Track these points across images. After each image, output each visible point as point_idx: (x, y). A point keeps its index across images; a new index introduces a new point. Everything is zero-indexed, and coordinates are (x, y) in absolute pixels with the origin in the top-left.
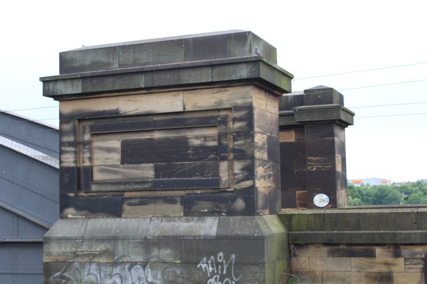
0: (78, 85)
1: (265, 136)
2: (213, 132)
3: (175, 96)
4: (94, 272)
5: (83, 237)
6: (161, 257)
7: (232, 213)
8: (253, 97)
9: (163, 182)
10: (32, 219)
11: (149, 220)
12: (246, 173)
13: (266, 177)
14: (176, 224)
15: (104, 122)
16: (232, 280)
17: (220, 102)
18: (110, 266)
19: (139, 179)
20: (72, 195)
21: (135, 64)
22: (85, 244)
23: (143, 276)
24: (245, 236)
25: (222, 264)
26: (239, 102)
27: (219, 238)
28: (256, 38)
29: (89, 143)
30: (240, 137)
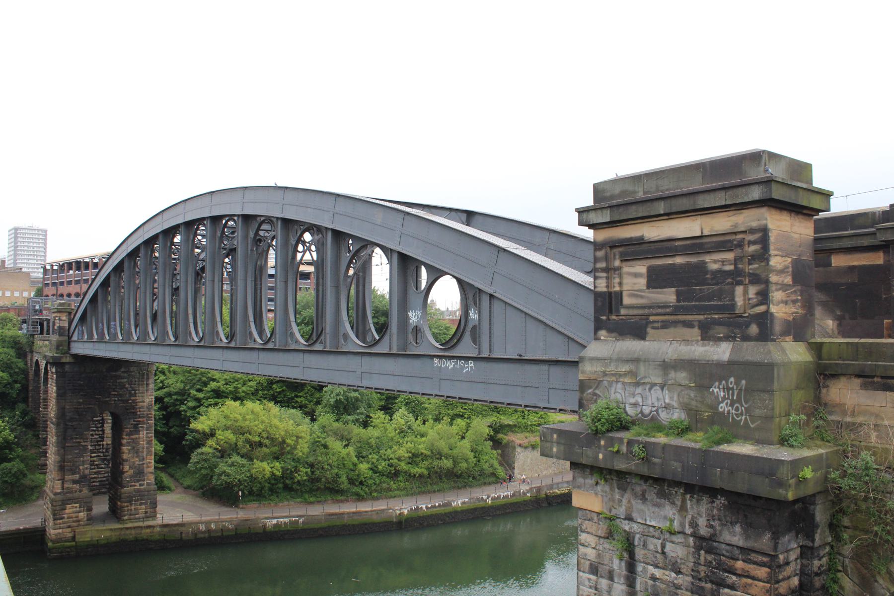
0: (606, 214)
1: (789, 260)
2: (730, 256)
3: (694, 220)
4: (620, 391)
5: (611, 358)
6: (677, 380)
7: (746, 338)
8: (768, 218)
9: (682, 307)
10: (579, 340)
11: (669, 344)
12: (760, 298)
13: (789, 302)
14: (693, 348)
15: (632, 248)
16: (742, 406)
17: (735, 226)
18: (633, 386)
19: (661, 303)
20: (604, 318)
21: (658, 191)
22: (612, 364)
23: (661, 397)
24: (756, 362)
25: (732, 389)
26: (754, 224)
27: (731, 363)
28: (773, 156)
29: (619, 268)
30: (754, 261)
